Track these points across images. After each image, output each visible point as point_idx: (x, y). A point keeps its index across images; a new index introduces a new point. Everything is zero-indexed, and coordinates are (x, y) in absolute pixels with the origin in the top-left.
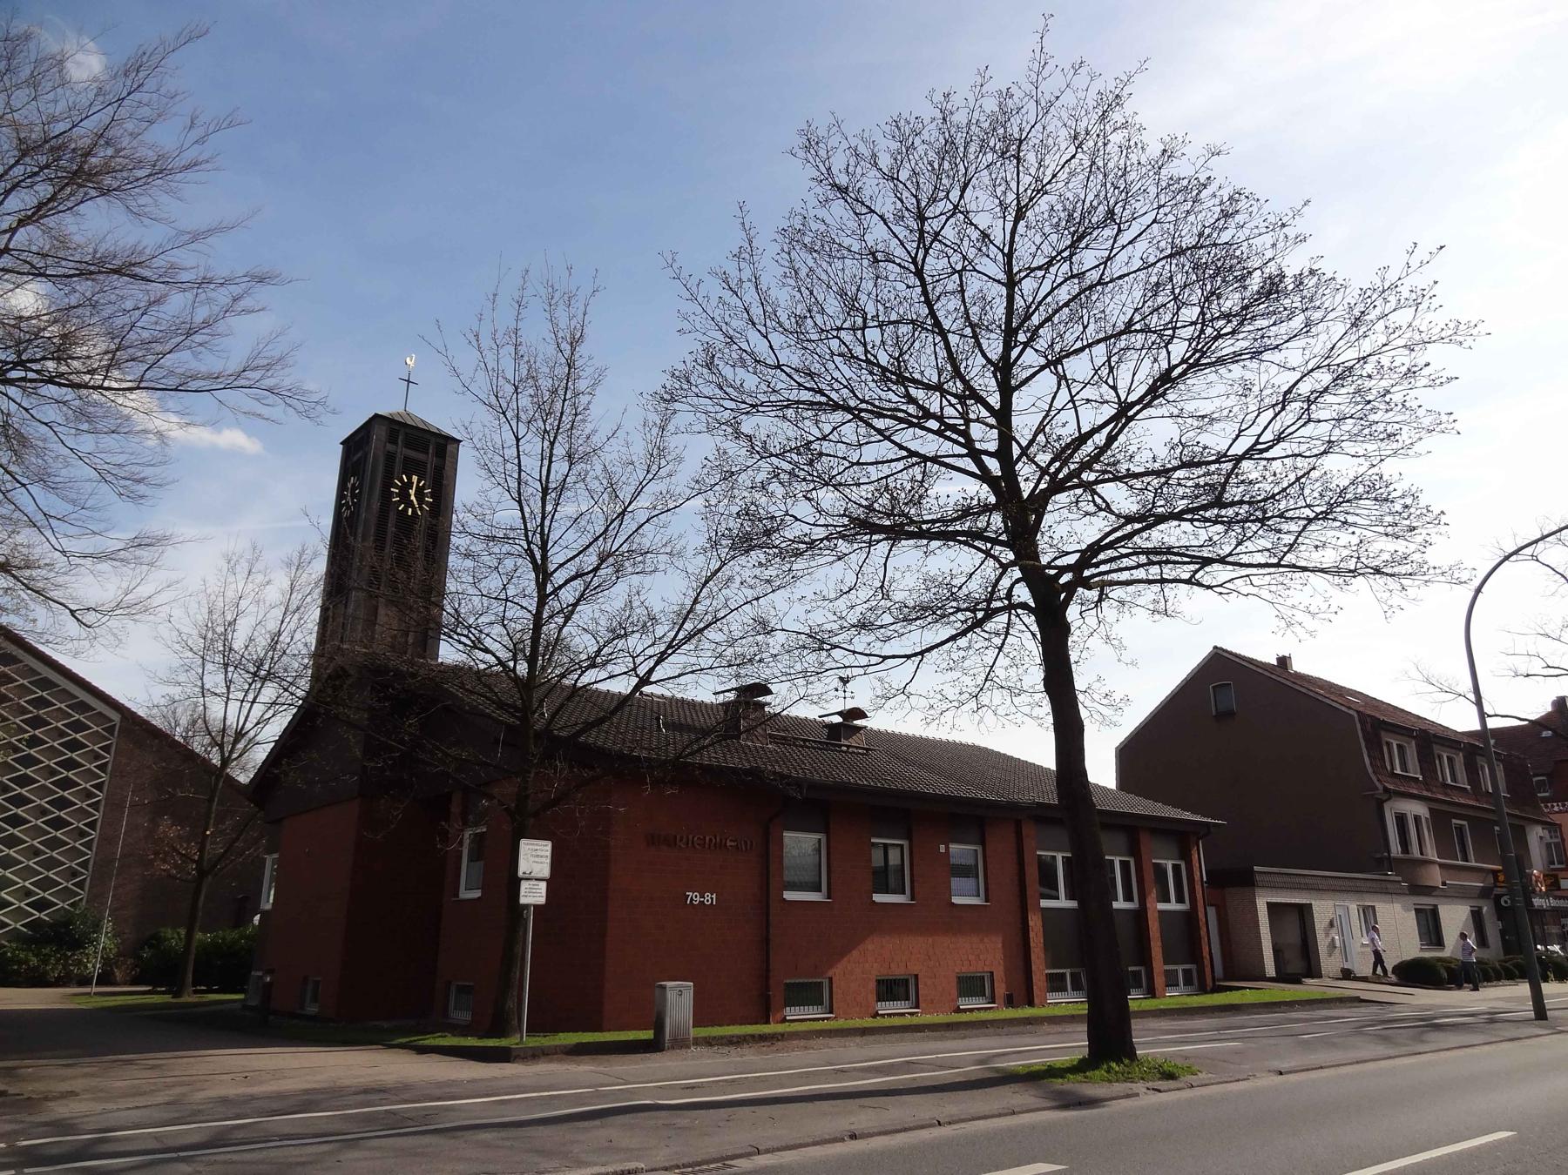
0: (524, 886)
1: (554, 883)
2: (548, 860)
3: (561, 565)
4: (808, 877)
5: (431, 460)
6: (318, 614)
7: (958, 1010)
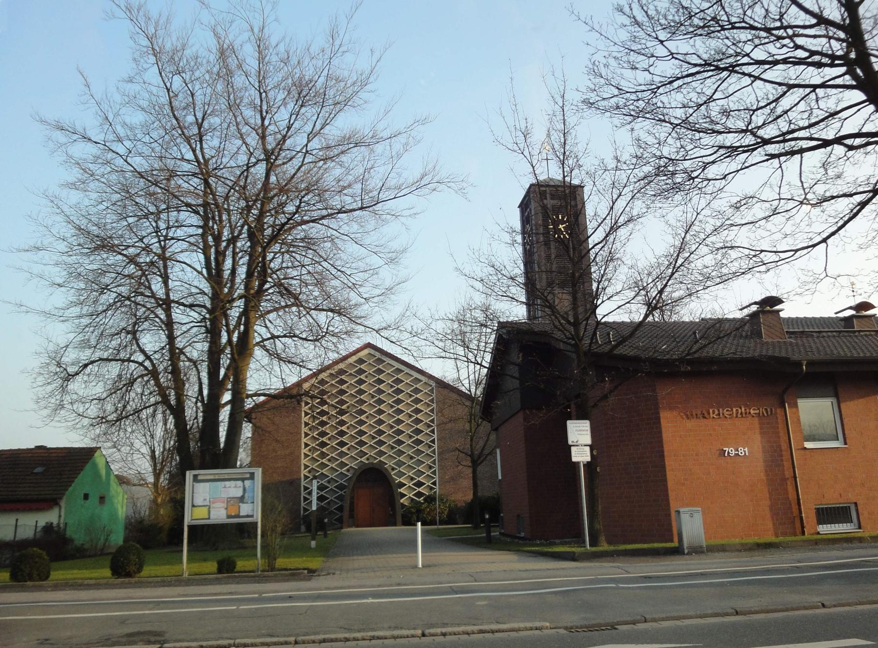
0: (573, 449)
2: (589, 433)
3: (323, 225)
4: (830, 430)
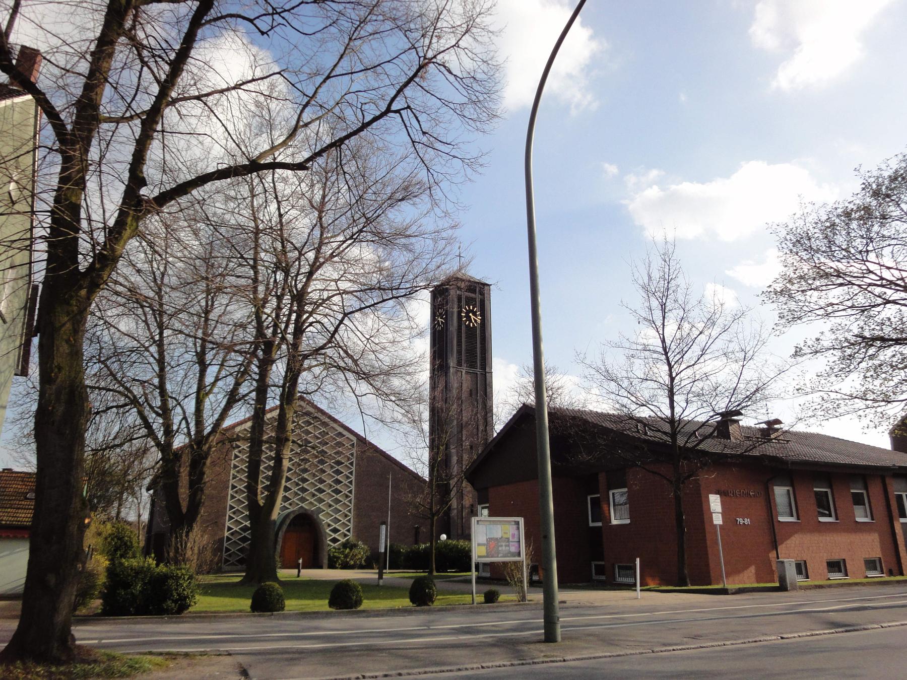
1: (724, 514)
5: (478, 297)
6: (38, 373)
7: (867, 577)
